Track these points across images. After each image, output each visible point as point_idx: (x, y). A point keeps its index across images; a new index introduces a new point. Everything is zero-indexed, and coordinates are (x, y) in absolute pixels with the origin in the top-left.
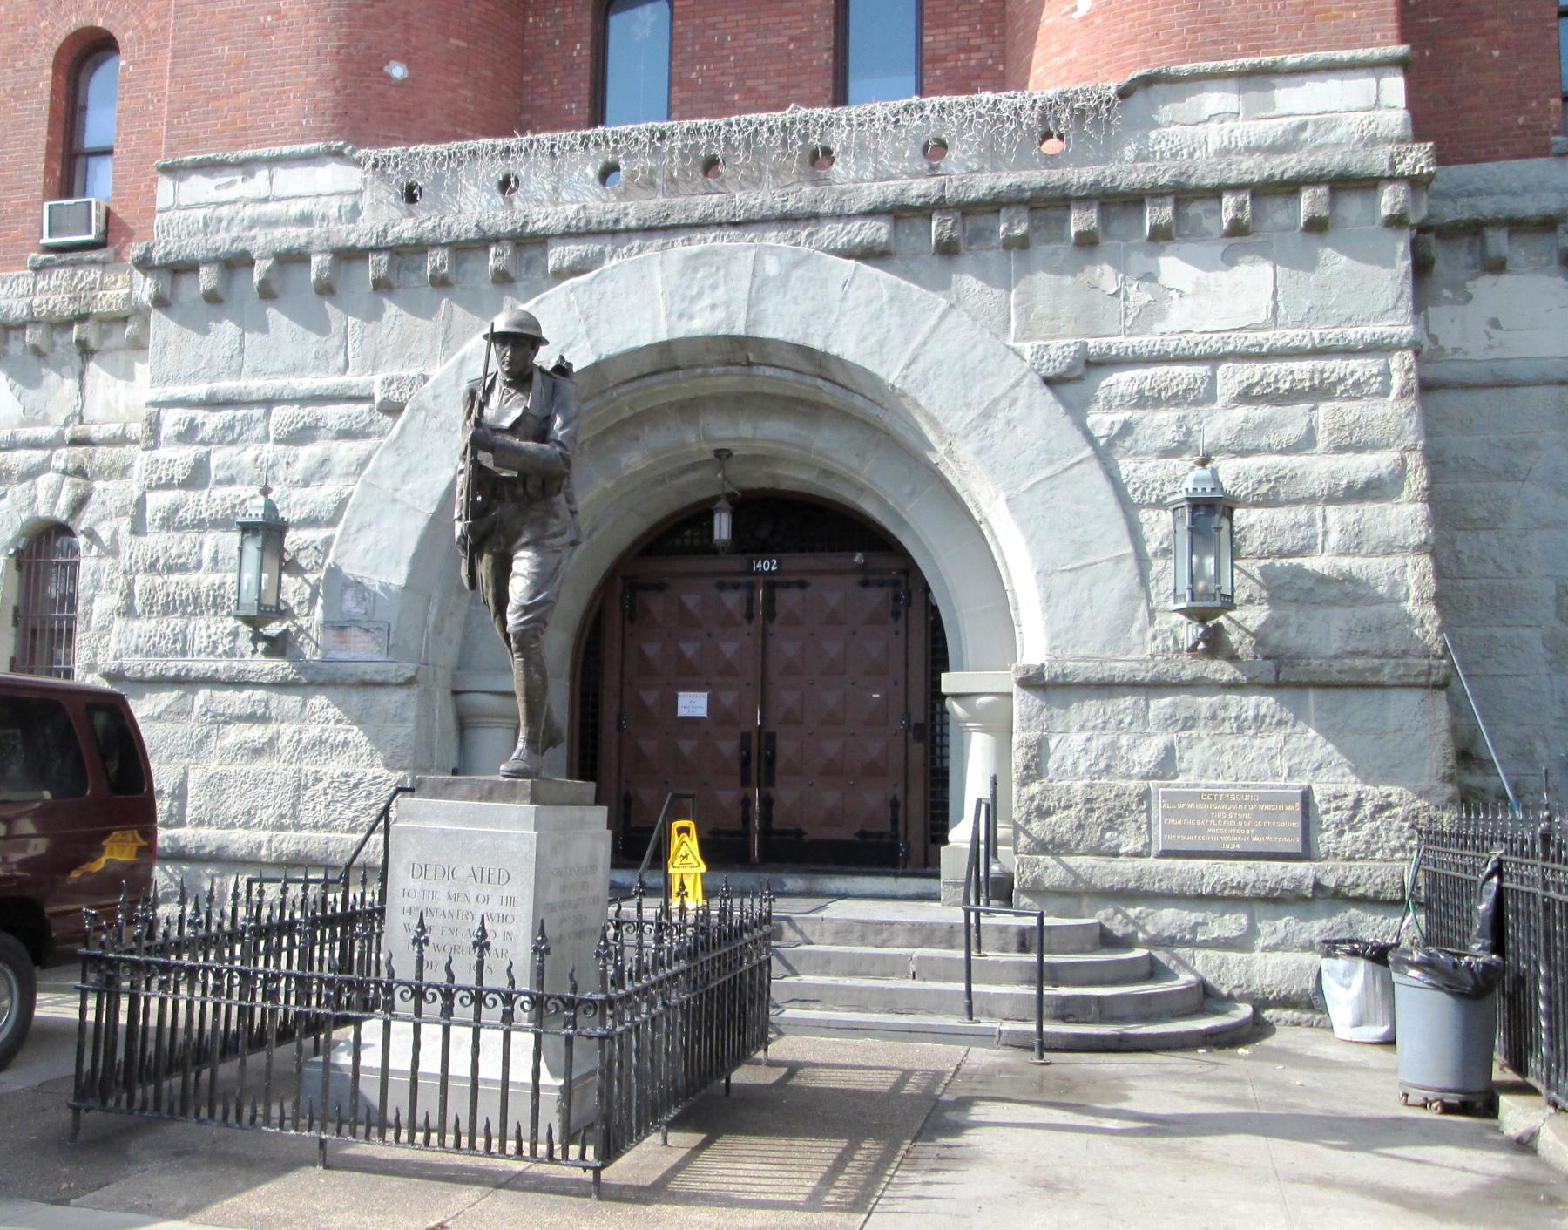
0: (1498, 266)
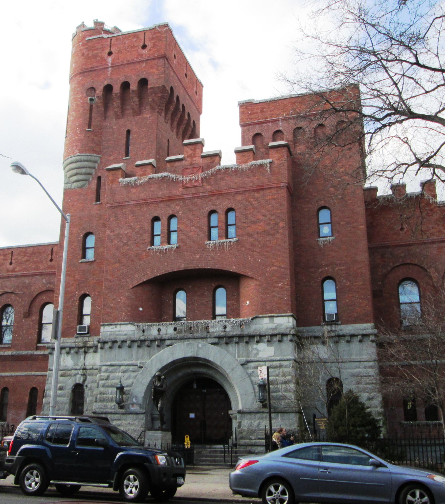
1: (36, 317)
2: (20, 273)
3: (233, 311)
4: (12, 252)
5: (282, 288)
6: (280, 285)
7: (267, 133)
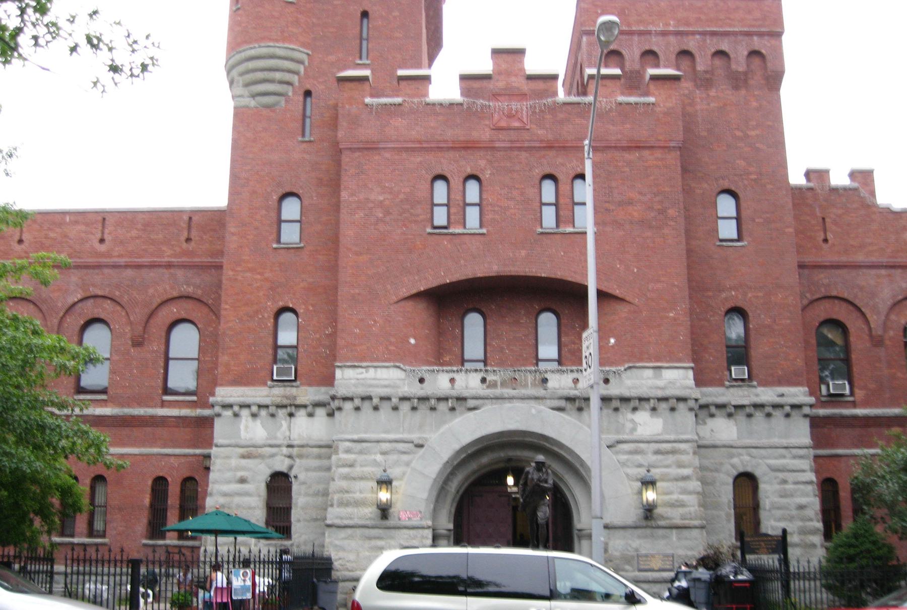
0: (712, 416)
1: (157, 346)
2: (123, 260)
3: (569, 356)
4: (104, 219)
5: (675, 319)
6: (671, 315)
7: (632, 52)
